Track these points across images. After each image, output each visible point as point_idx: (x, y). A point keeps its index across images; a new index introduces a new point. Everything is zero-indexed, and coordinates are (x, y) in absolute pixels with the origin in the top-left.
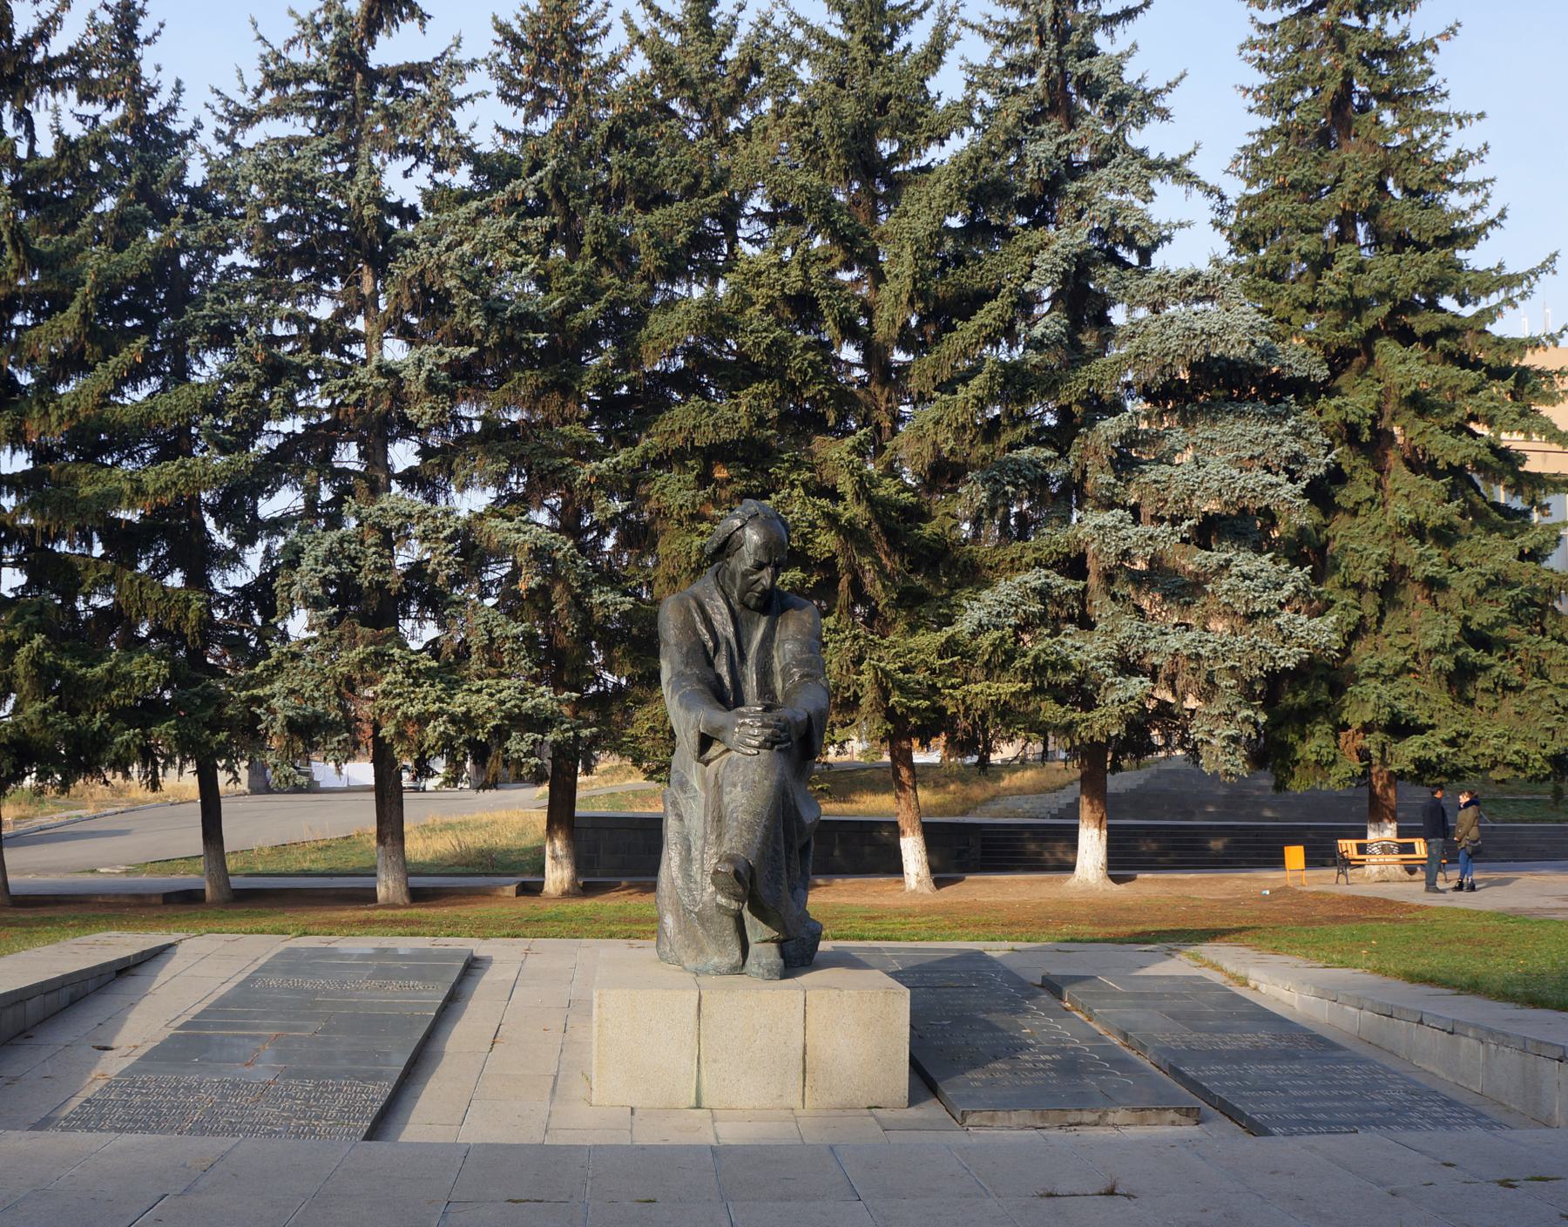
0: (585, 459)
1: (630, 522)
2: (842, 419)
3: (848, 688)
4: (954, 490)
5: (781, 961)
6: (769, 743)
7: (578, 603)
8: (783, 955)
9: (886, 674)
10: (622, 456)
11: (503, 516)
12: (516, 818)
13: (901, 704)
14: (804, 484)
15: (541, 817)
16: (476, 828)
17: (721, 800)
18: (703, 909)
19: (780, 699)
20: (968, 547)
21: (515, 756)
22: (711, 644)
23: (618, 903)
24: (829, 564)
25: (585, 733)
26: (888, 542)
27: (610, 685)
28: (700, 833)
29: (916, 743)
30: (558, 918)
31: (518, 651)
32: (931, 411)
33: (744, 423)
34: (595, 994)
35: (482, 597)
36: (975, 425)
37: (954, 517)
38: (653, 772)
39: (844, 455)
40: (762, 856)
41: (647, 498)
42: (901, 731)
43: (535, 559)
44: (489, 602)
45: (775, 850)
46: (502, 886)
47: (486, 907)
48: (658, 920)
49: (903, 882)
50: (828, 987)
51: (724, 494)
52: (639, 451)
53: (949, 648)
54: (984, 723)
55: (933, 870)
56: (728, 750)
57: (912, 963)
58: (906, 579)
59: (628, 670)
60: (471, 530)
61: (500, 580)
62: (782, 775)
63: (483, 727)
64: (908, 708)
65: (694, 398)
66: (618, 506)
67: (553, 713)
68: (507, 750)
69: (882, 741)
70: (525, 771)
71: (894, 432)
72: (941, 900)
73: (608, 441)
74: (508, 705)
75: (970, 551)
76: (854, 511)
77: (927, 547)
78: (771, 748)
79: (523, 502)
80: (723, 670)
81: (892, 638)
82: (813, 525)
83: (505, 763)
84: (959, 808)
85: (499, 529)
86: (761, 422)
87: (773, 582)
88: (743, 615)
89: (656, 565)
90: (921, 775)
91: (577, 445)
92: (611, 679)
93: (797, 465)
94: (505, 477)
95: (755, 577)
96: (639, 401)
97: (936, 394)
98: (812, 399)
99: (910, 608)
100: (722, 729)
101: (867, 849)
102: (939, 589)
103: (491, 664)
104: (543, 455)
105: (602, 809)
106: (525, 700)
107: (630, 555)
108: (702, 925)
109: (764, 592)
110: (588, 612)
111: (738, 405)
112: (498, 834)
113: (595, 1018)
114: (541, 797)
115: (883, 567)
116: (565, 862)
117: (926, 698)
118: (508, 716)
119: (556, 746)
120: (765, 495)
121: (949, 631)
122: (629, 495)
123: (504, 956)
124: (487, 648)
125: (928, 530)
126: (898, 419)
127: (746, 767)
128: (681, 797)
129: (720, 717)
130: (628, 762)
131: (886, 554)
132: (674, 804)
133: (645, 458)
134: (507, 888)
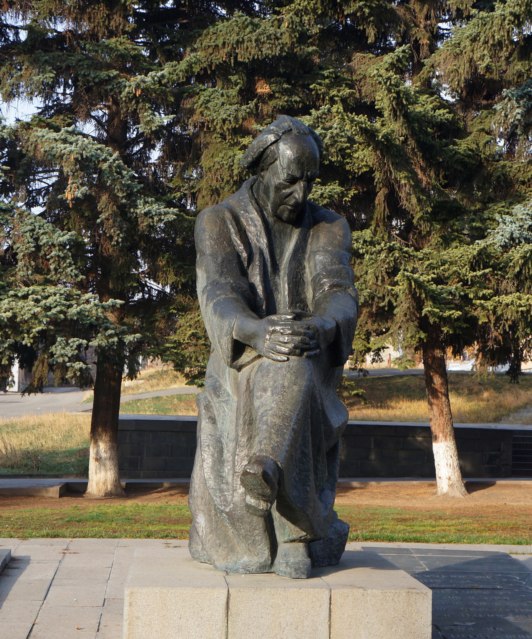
0: (131, 72)
1: (175, 135)
2: (382, 36)
3: (383, 298)
4: (488, 107)
5: (308, 561)
6: (299, 350)
7: (123, 213)
8: (310, 554)
9: (420, 285)
10: (167, 70)
11: (50, 126)
12: (63, 421)
13: (434, 314)
14: (344, 101)
15: (87, 419)
16: (23, 430)
17: (252, 404)
18: (234, 509)
19: (311, 308)
20: (502, 163)
21: (60, 360)
22: (245, 255)
23: (158, 504)
24: (366, 179)
25: (129, 338)
26: (424, 158)
27: (154, 293)
28: (232, 435)
29: (449, 351)
30: (100, 518)
31: (64, 258)
32: (468, 29)
33: (286, 39)
34: (127, 592)
35: (30, 205)
36: (512, 42)
37: (488, 133)
38: (195, 377)
39: (383, 72)
40: (290, 458)
41: (191, 112)
42: (433, 341)
43: (81, 169)
44: (37, 210)
45: (303, 453)
46: (46, 488)
47: (28, 509)
48: (191, 520)
49: (435, 485)
50: (352, 586)
51: (266, 109)
52: (183, 65)
53: (481, 260)
54: (514, 333)
55: (464, 474)
56: (259, 356)
57: (439, 564)
58: (441, 193)
59: (172, 278)
60: (17, 139)
61: (47, 189)
62: (311, 380)
63: (28, 333)
64: (441, 318)
65: (237, 13)
66: (164, 119)
67: (98, 319)
68: (52, 355)
69: (416, 349)
70: (69, 375)
71: (432, 49)
72: (472, 504)
73: (153, 55)
74: (54, 311)
75: (504, 166)
76: (391, 127)
77: (462, 162)
78: (300, 355)
79: (70, 112)
80: (256, 280)
81: (426, 250)
82: (351, 140)
83: (51, 367)
84: (492, 415)
85: (45, 139)
86: (303, 38)
87: (305, 195)
88: (276, 227)
89: (201, 176)
90: (456, 383)
91: (123, 57)
92: (155, 286)
93: (337, 81)
94: (52, 87)
95: (288, 191)
96: (184, 15)
97: (474, 11)
98: (353, 16)
99: (444, 222)
100: (253, 336)
101: (402, 454)
102: (473, 203)
103: (37, 270)
104: (89, 67)
105: (147, 413)
106: (70, 306)
107: (175, 167)
108: (233, 524)
109: (297, 205)
110: (133, 222)
111: (280, 21)
112: (44, 436)
113: (125, 617)
114: (88, 401)
115: (418, 182)
116: (109, 464)
117: (458, 308)
118: (54, 321)
119: (101, 351)
120: (306, 111)
121: (481, 243)
122: (174, 108)
123: (40, 555)
124: (33, 256)
125: (463, 146)
126: (436, 36)
127: (276, 373)
128: (214, 401)
129: (252, 325)
130: (171, 366)
131: (422, 169)
132: (208, 407)
133: (189, 72)
134: (51, 489)
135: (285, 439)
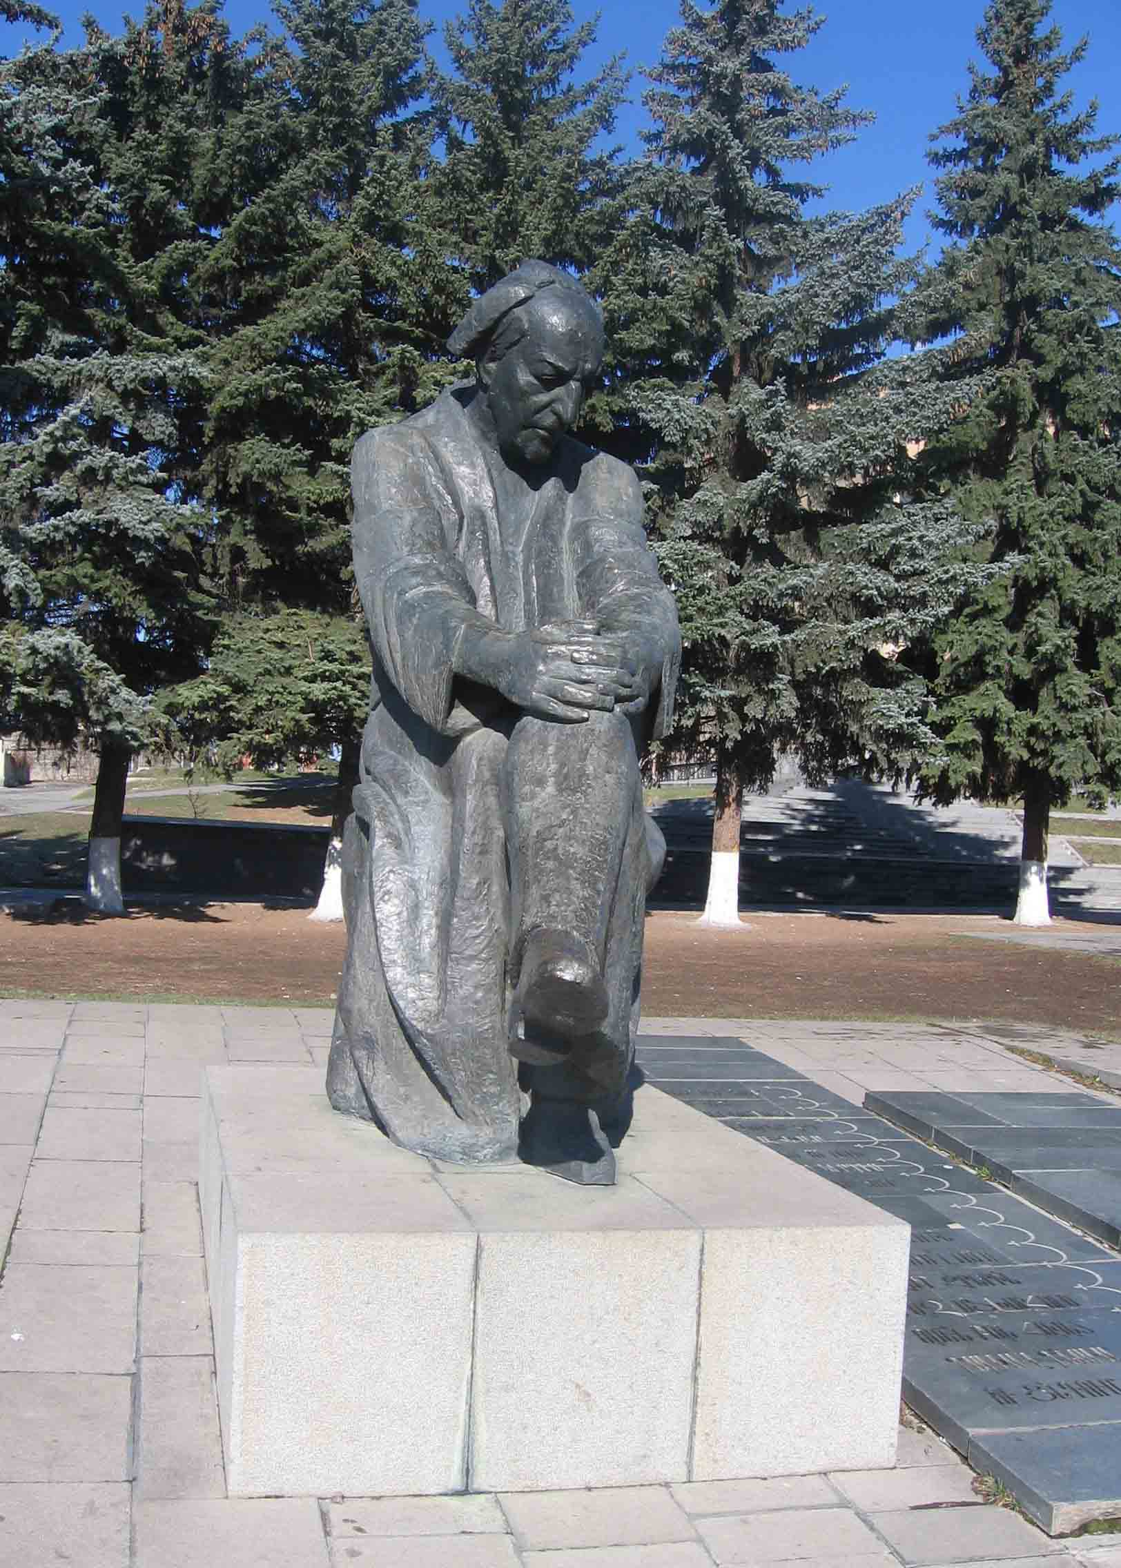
135: (598, 892)
